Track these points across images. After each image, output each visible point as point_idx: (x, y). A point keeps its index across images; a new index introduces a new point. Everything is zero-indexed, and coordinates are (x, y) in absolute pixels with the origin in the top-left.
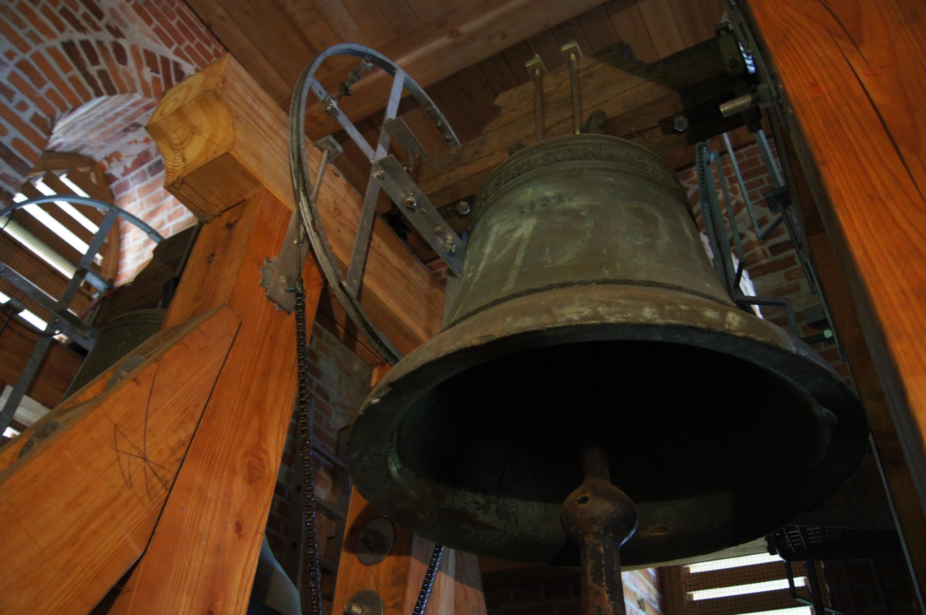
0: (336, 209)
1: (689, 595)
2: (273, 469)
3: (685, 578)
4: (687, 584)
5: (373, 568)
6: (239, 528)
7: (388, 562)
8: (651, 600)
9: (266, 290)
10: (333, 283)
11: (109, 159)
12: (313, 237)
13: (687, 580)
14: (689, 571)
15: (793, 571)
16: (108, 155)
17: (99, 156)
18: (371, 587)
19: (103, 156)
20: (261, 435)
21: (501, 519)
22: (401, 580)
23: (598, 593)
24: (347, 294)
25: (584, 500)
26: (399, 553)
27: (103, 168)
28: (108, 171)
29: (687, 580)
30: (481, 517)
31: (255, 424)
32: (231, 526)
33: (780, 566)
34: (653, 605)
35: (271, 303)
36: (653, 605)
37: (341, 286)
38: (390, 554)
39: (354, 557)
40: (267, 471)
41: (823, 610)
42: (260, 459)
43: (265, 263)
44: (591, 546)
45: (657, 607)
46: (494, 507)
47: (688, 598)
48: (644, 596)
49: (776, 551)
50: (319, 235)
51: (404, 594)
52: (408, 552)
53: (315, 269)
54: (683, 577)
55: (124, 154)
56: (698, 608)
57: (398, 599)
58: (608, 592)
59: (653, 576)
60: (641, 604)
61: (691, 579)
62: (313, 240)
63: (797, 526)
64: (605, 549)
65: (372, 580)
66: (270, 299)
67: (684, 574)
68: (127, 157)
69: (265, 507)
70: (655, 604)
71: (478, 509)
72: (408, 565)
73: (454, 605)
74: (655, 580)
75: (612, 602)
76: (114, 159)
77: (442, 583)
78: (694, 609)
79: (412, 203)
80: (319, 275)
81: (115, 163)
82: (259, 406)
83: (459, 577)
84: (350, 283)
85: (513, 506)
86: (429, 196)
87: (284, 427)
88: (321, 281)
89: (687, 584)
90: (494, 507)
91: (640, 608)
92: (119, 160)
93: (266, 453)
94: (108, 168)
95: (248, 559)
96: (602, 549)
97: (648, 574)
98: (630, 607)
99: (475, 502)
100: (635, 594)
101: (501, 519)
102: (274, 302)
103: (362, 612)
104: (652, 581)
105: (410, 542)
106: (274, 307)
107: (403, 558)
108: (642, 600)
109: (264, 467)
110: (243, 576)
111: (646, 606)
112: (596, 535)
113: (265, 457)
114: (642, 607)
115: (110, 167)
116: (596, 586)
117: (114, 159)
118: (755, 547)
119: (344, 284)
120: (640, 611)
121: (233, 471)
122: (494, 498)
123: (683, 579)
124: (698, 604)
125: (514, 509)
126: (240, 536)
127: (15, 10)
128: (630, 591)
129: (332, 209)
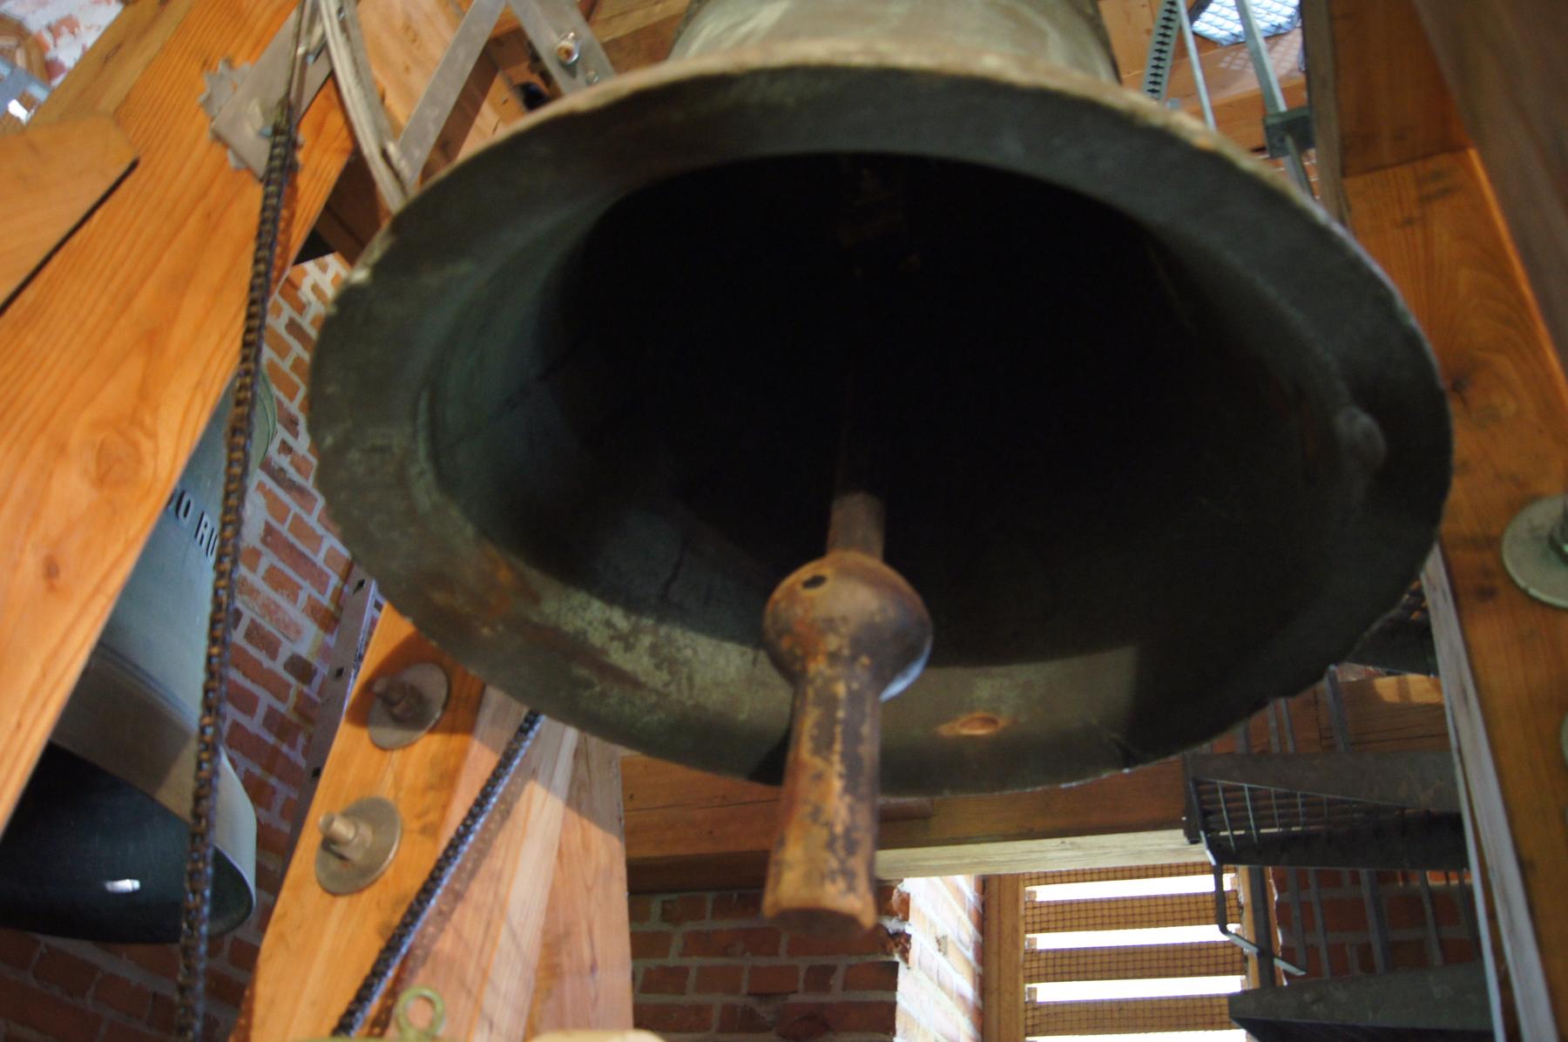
0: (407, 28)
1: (1030, 939)
2: (163, 474)
3: (1026, 909)
4: (1029, 920)
5: (396, 756)
6: (51, 570)
7: (428, 746)
8: (960, 941)
9: (212, 120)
10: (370, 148)
11: (54, 30)
12: (336, 43)
13: (1029, 913)
14: (1035, 897)
15: (1228, 913)
16: (53, 22)
17: (36, 22)
18: (386, 791)
19: (44, 22)
20: (145, 394)
21: (658, 667)
22: (447, 779)
23: (819, 777)
24: (397, 175)
25: (816, 581)
26: (452, 730)
27: (41, 47)
28: (50, 55)
29: (1029, 913)
30: (617, 656)
31: (133, 369)
32: (31, 564)
33: (1205, 902)
34: (963, 949)
35: (218, 148)
36: (963, 949)
37: (385, 155)
38: (432, 731)
39: (364, 735)
40: (148, 472)
41: (1272, 962)
42: (135, 445)
43: (221, 67)
44: (819, 682)
45: (970, 954)
46: (647, 640)
47: (1026, 944)
48: (948, 932)
49: (1199, 837)
50: (348, 38)
51: (445, 807)
52: (469, 728)
53: (336, 120)
54: (1022, 907)
55: (84, 21)
56: (1042, 963)
57: (433, 817)
58: (841, 776)
59: (969, 900)
60: (941, 943)
61: (1037, 912)
62: (338, 50)
63: (1246, 785)
64: (850, 692)
65: (389, 779)
66: (218, 138)
67: (1026, 902)
68: (89, 28)
69: (128, 547)
70: (967, 949)
71: (612, 638)
72: (463, 753)
73: (555, 853)
74: (972, 908)
75: (848, 799)
76: (65, 30)
77: (535, 807)
78: (1035, 964)
79: (569, 53)
80: (345, 133)
81: (65, 39)
82: (152, 340)
83: (578, 799)
84: (405, 151)
85: (686, 646)
86: (607, 47)
87: (205, 397)
88: (348, 145)
89: (1029, 920)
90: (647, 640)
91: (940, 950)
92: (73, 33)
93: (152, 436)
94: (52, 46)
95: (64, 640)
96: (841, 689)
97: (958, 891)
98: (921, 945)
99: (608, 624)
100: (932, 924)
101: (658, 667)
102: (226, 145)
103: (355, 836)
104: (967, 908)
105: (476, 705)
106: (226, 160)
107: (456, 741)
108: (945, 937)
109: (139, 461)
110: (44, 674)
111: (950, 949)
112: (834, 657)
113: (146, 445)
114: (943, 950)
115: (55, 46)
116: (818, 763)
117: (65, 30)
118: (1157, 851)
119: (392, 149)
120: (939, 956)
121: (60, 449)
122: (648, 622)
123: (1022, 912)
124: (1043, 956)
125: (688, 653)
126: (52, 588)
127: (283, 332)
128: (924, 917)
129: (399, 23)
